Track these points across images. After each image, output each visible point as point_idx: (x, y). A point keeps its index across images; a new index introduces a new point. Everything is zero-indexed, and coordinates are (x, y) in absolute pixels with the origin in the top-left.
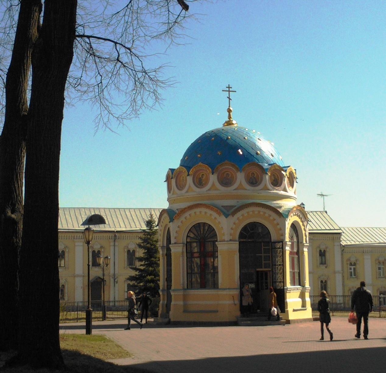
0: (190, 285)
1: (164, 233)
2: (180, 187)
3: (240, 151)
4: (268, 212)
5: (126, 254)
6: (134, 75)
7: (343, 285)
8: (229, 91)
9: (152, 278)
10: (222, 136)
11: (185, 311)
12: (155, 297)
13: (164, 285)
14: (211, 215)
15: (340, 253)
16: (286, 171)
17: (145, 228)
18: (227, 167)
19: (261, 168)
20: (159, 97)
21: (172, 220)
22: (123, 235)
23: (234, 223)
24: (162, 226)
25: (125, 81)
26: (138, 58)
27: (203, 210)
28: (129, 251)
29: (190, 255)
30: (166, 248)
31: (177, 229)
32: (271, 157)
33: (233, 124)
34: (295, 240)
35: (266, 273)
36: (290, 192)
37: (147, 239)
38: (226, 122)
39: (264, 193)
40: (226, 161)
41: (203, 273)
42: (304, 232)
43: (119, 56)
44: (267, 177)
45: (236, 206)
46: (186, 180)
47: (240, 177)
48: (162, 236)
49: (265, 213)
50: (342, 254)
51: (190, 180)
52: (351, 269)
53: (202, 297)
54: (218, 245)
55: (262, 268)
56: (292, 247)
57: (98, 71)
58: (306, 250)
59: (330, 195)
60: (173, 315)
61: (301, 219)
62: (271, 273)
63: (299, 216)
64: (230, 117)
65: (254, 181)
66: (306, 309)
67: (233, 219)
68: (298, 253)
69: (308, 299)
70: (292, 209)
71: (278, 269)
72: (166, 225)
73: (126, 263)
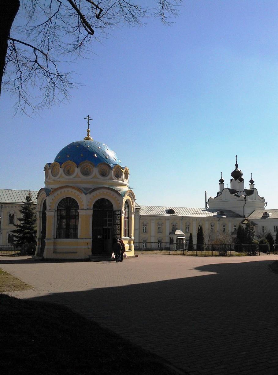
0: (59, 236)
1: (41, 203)
2: (54, 175)
3: (95, 155)
4: (113, 193)
5: (8, 217)
6: (48, 75)
7: (139, 237)
8: (89, 119)
9: (28, 231)
10: (84, 145)
11: (55, 252)
12: (30, 243)
13: (40, 236)
14: (75, 193)
15: (138, 219)
16: (124, 169)
17: (26, 201)
18: (87, 164)
19: (110, 166)
20: (68, 94)
21: (48, 195)
22: (6, 205)
23: (91, 199)
24: (40, 199)
25: (40, 78)
26: (53, 62)
27: (70, 190)
28: (10, 215)
29: (60, 218)
30: (42, 213)
31: (51, 201)
32: (114, 160)
33: (91, 139)
34: (127, 210)
35: (109, 229)
36: (126, 182)
37: (27, 208)
38: (86, 138)
39: (110, 182)
40: (87, 161)
41: (67, 229)
42: (132, 206)
43: (37, 59)
44: (113, 172)
45: (92, 188)
46: (59, 171)
47: (95, 171)
48: (40, 205)
49: (110, 193)
50: (139, 220)
51: (61, 170)
52: (144, 228)
53: (66, 244)
54: (79, 212)
55: (106, 226)
56: (125, 214)
57: (19, 68)
58: (133, 216)
59: (134, 188)
60: (46, 255)
61: (131, 198)
62: (112, 230)
63: (130, 196)
64: (88, 135)
65: (104, 174)
66: (131, 251)
67: (90, 196)
68: (128, 218)
69: (132, 245)
70: (127, 192)
71: (117, 227)
72: (43, 198)
73: (8, 222)
